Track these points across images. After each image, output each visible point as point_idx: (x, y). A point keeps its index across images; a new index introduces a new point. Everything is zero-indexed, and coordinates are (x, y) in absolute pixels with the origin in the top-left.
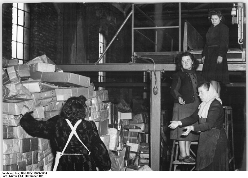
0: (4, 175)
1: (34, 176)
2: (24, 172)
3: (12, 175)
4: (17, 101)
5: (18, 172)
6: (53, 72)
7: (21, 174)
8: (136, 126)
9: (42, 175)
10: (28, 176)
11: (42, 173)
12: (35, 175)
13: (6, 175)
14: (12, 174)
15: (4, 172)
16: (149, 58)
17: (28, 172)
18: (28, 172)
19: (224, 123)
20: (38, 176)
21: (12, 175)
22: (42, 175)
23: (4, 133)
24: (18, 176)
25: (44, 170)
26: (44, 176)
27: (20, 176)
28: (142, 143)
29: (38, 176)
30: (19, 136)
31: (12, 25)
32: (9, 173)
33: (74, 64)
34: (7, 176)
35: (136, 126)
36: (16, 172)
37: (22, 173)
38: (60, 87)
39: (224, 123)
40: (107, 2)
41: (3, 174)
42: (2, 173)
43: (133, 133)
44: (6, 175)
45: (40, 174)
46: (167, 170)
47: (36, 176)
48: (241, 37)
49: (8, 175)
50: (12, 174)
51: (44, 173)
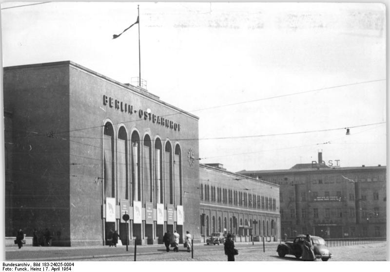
0: (7, 267)
1: (22, 269)
2: (38, 262)
9: (66, 267)
11: (67, 264)
13: (9, 267)
14: (19, 265)
15: (7, 263)
17: (44, 262)
19: (35, 244)
22: (66, 267)
23: (12, 208)
24: (42, 269)
25: (277, 246)
28: (328, 256)
31: (68, 171)
32: (14, 265)
33: (192, 255)
36: (25, 262)
37: (34, 265)
39: (35, 244)
41: (5, 266)
42: (4, 264)
44: (9, 267)
45: (63, 266)
46: (383, 223)
47: (22, 269)
49: (13, 267)
50: (19, 265)
51: (69, 264)
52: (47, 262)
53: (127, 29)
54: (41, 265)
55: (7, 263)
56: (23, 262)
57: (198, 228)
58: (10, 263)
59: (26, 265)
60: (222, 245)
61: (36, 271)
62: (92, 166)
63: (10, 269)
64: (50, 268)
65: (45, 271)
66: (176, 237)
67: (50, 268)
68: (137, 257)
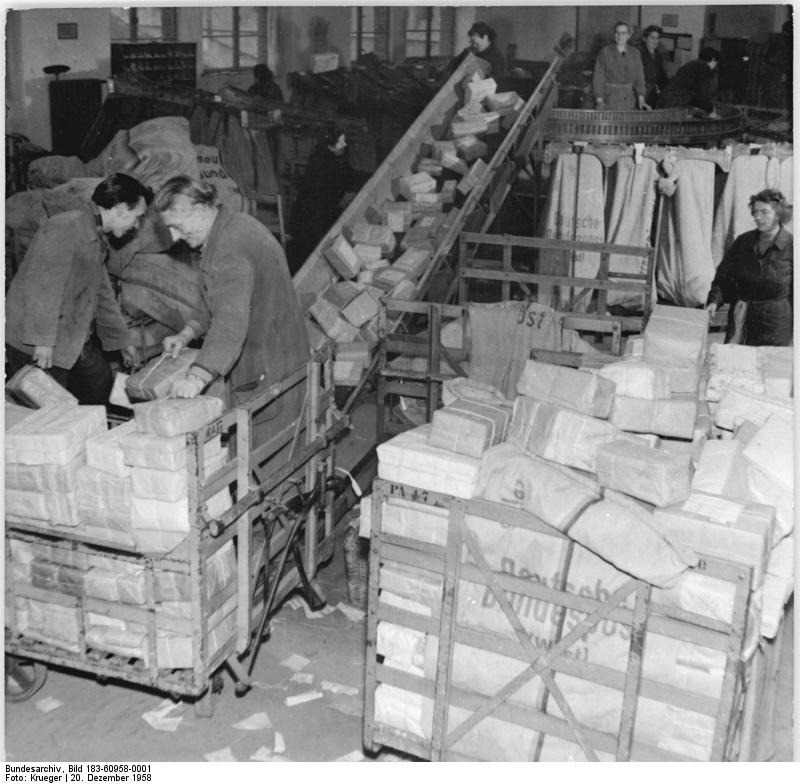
0: (14, 774)
1: (117, 778)
3: (38, 774)
4: (680, 262)
5: (58, 764)
6: (384, 685)
7: (67, 771)
8: (447, 230)
9: (142, 773)
10: (96, 778)
11: (136, 768)
12: (120, 774)
13: (19, 774)
14: (39, 770)
16: (488, 419)
17: (90, 764)
18: (90, 764)
20: (130, 780)
21: (38, 774)
26: (147, 769)
27: (70, 778)
29: (130, 780)
30: (180, 309)
32: (28, 769)
34: (21, 779)
35: (447, 230)
37: (71, 768)
38: (634, 304)
40: (794, 91)
41: (10, 772)
42: (8, 768)
43: (269, 12)
44: (19, 774)
48: (466, 398)
49: (27, 775)
50: (39, 770)
51: (142, 769)
52: (96, 764)
53: (602, 558)
54: (85, 769)
55: (13, 765)
56: (46, 764)
57: (363, 317)
58: (21, 765)
59: (54, 770)
60: (242, 34)
61: (107, 782)
62: (301, 169)
63: (21, 779)
64: (84, 775)
65: (69, 781)
66: (334, 686)
67: (84, 775)
68: (544, 750)
